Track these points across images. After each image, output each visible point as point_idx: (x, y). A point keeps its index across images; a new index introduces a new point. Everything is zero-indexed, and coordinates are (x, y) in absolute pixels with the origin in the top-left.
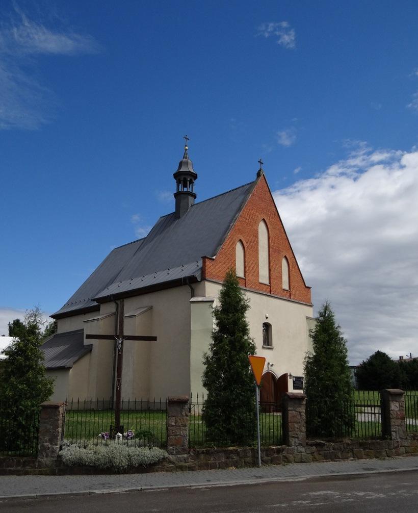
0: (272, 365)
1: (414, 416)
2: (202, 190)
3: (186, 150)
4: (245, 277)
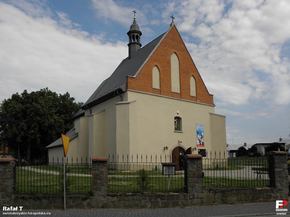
0: (181, 142)
1: (33, 173)
2: (144, 41)
3: (135, 18)
4: (160, 88)
